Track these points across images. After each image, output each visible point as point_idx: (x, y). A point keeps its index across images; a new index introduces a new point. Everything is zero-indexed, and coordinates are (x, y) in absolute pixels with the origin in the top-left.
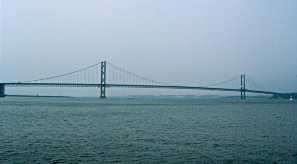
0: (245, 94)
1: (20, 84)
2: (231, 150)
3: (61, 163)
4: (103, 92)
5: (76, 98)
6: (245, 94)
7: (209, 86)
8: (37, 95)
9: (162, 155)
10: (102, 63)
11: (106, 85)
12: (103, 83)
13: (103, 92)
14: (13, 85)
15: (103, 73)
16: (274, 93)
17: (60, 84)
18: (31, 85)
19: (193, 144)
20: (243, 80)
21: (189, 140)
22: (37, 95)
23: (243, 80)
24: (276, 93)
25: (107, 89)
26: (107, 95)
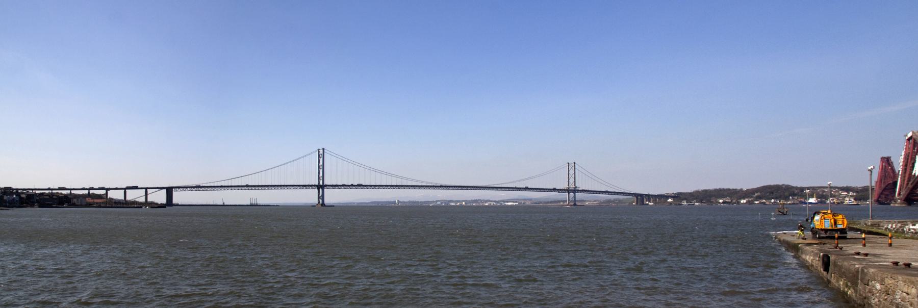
0: (575, 197)
1: (247, 186)
2: (21, 293)
3: (517, 307)
4: (321, 197)
5: (337, 206)
6: (575, 197)
7: (505, 183)
8: (224, 203)
9: (335, 300)
10: (319, 150)
11: (326, 186)
12: (321, 183)
13: (321, 197)
14: (200, 189)
15: (321, 167)
16: (636, 195)
17: (501, 188)
18: (225, 188)
19: (378, 285)
20: (572, 172)
21: (549, 280)
22: (224, 203)
23: (572, 172)
24: (641, 195)
25: (326, 191)
26: (175, 201)
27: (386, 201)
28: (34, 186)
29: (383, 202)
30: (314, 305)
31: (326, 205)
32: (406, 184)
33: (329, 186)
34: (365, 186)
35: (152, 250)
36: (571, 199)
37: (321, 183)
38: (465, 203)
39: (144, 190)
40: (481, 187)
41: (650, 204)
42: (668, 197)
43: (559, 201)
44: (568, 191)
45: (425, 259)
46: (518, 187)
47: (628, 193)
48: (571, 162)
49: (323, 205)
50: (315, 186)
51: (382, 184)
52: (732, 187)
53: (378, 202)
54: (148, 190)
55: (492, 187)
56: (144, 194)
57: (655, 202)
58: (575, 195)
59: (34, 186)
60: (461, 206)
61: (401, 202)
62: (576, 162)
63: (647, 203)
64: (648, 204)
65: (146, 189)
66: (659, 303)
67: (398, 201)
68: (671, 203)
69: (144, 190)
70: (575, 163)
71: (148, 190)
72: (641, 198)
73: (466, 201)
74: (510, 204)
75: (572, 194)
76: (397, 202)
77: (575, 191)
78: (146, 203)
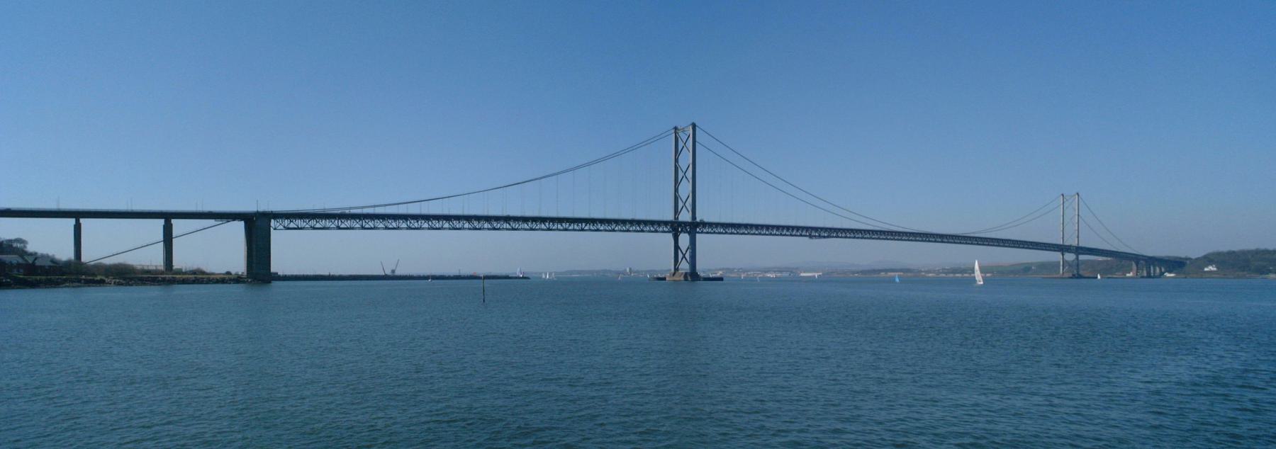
11: (704, 224)
26: (279, 263)
30: (632, 446)
31: (702, 275)
33: (711, 225)
37: (685, 216)
39: (161, 223)
40: (778, 227)
45: (219, 435)
48: (683, 123)
49: (693, 275)
50: (666, 223)
52: (1023, 239)
54: (174, 221)
56: (160, 237)
65: (168, 217)
66: (993, 389)
67: (630, 269)
69: (162, 222)
70: (694, 126)
71: (174, 221)
73: (651, 271)
74: (930, 275)
76: (628, 270)
78: (167, 277)
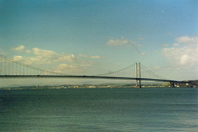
1: (6, 76)
6: (140, 82)
16: (170, 81)
27: (29, 86)
28: (9, 74)
29: (27, 87)
32: (12, 75)
34: (9, 76)
35: (41, 120)
36: (138, 84)
38: (78, 87)
40: (90, 77)
41: (177, 86)
42: (185, 82)
43: (130, 85)
44: (137, 79)
46: (108, 76)
47: (161, 80)
51: (21, 75)
53: (25, 87)
55: (96, 77)
57: (179, 85)
58: (140, 81)
59: (9, 74)
60: (76, 88)
61: (40, 87)
62: (141, 63)
63: (176, 86)
64: (176, 87)
67: (38, 86)
68: (188, 86)
72: (173, 83)
75: (138, 81)
77: (140, 79)
